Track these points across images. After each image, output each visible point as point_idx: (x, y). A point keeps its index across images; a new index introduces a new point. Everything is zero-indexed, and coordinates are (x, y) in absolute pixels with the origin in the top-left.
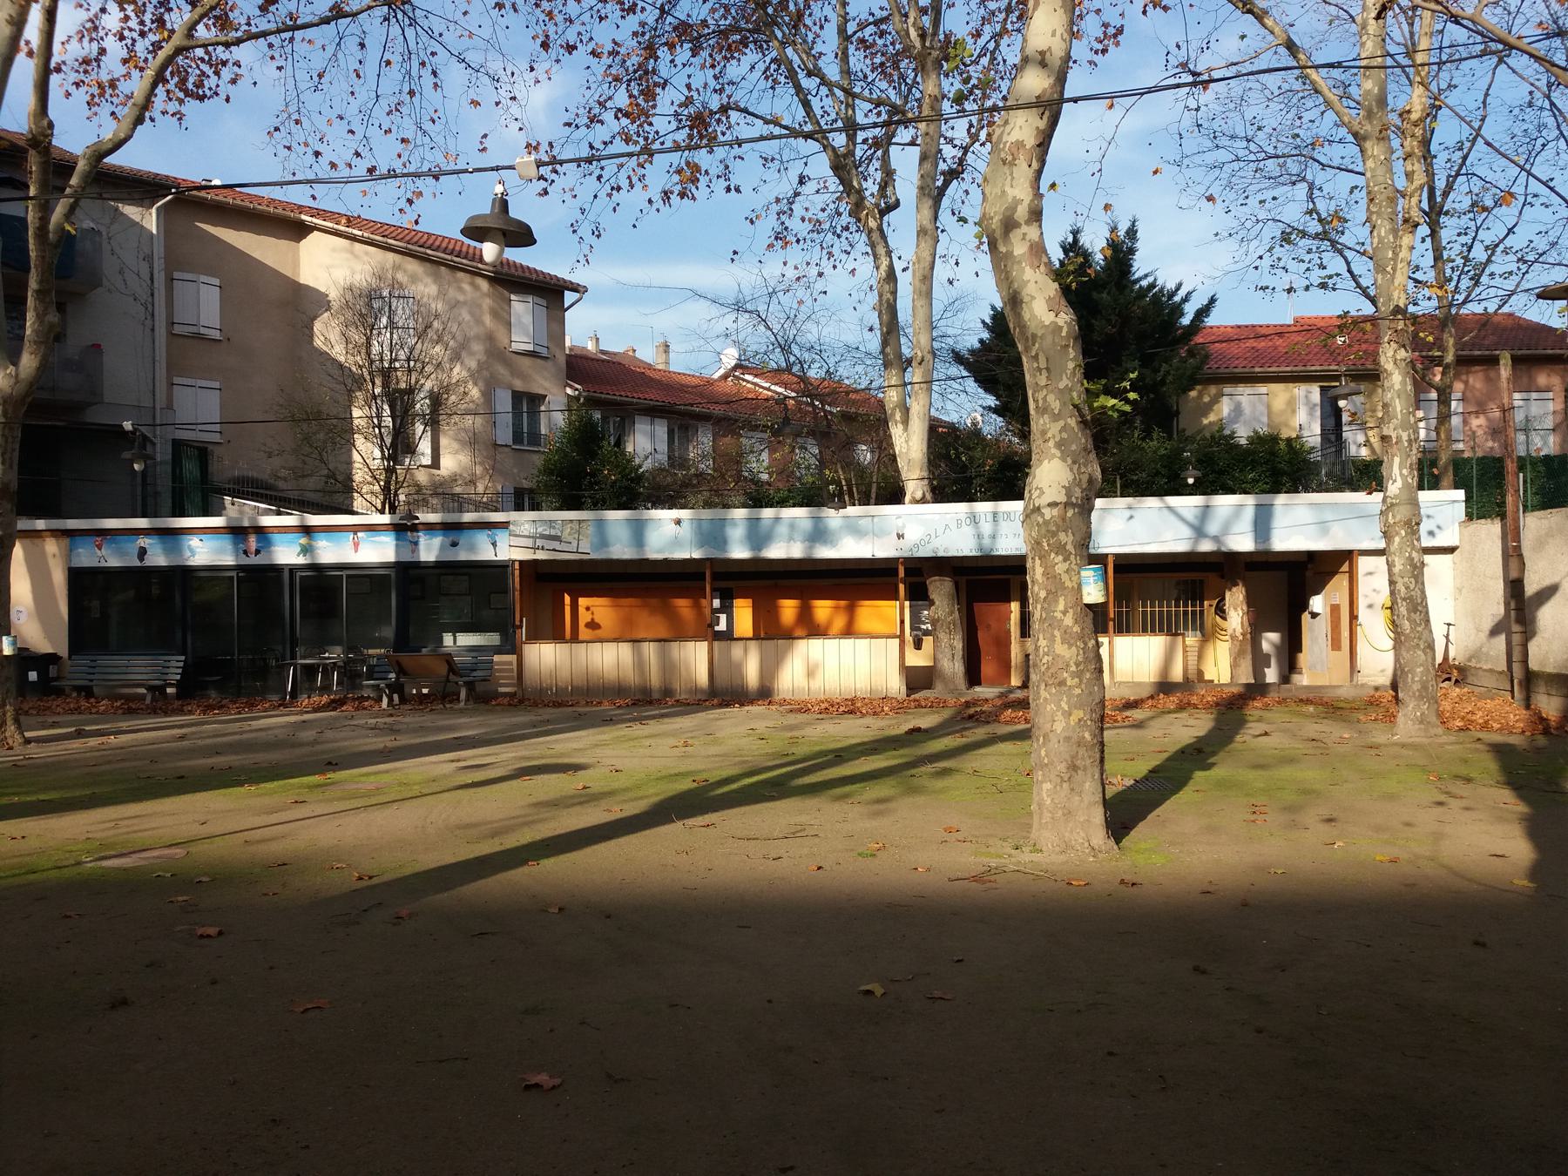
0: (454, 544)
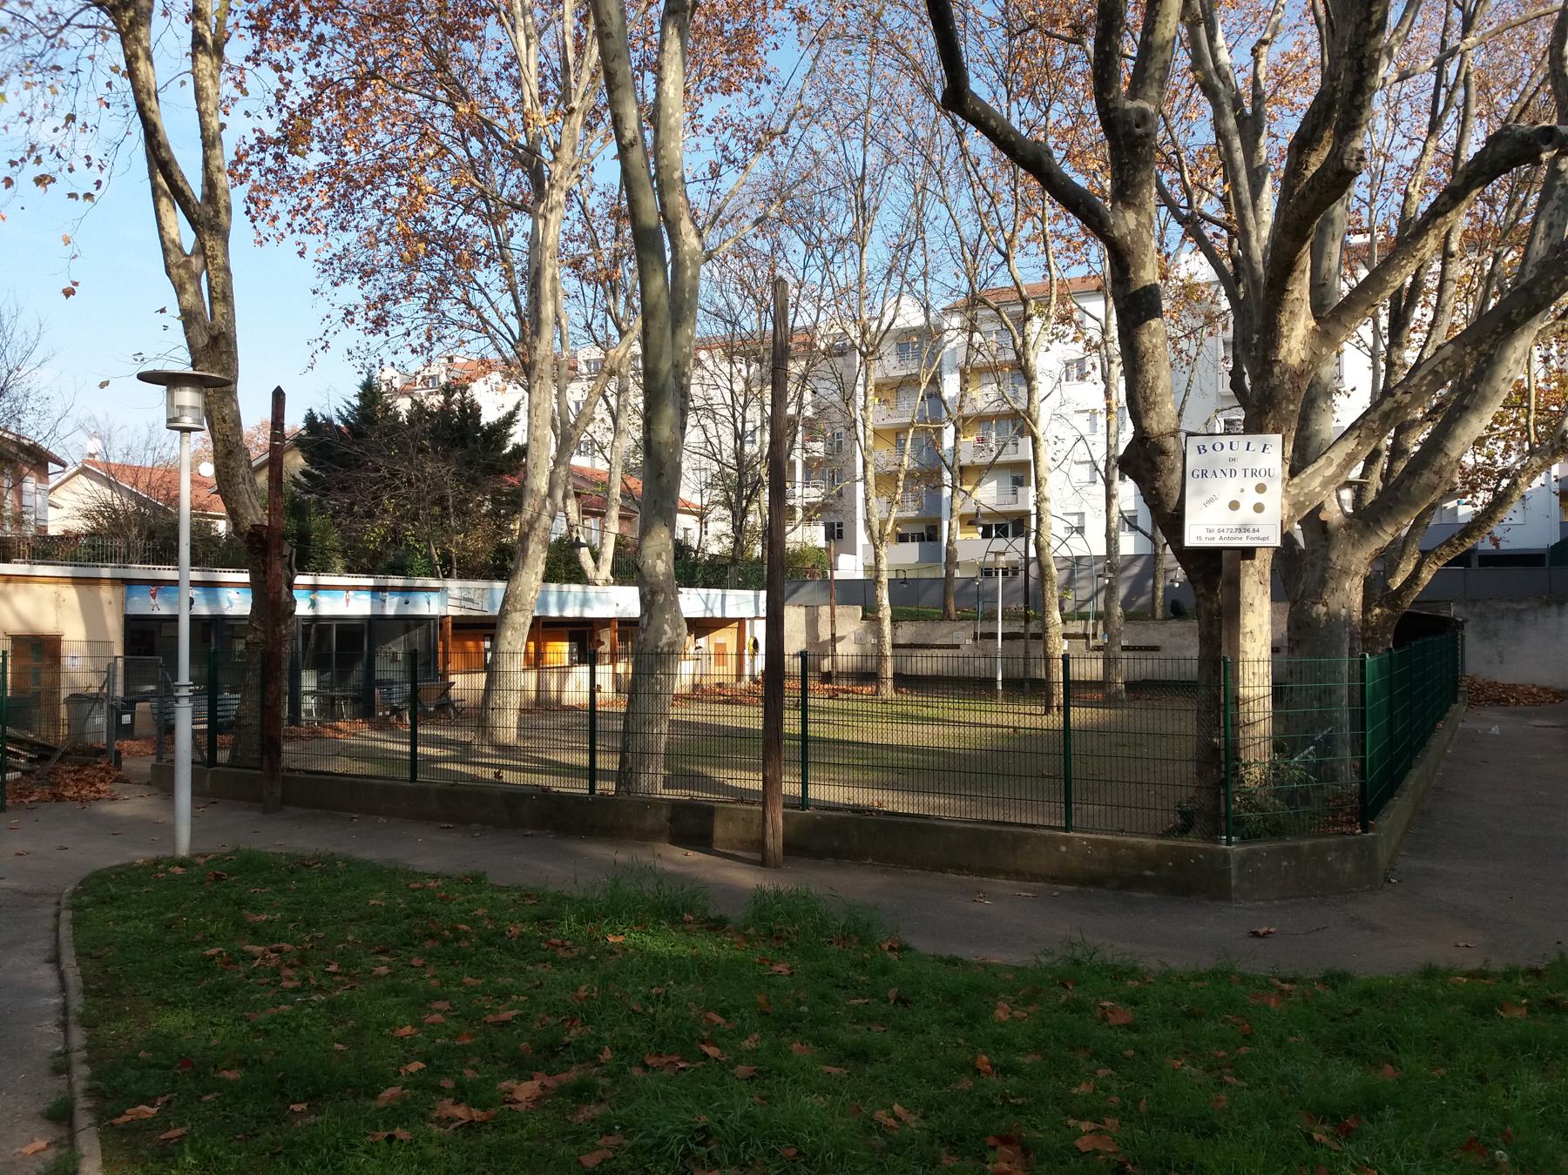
0: (407, 603)
